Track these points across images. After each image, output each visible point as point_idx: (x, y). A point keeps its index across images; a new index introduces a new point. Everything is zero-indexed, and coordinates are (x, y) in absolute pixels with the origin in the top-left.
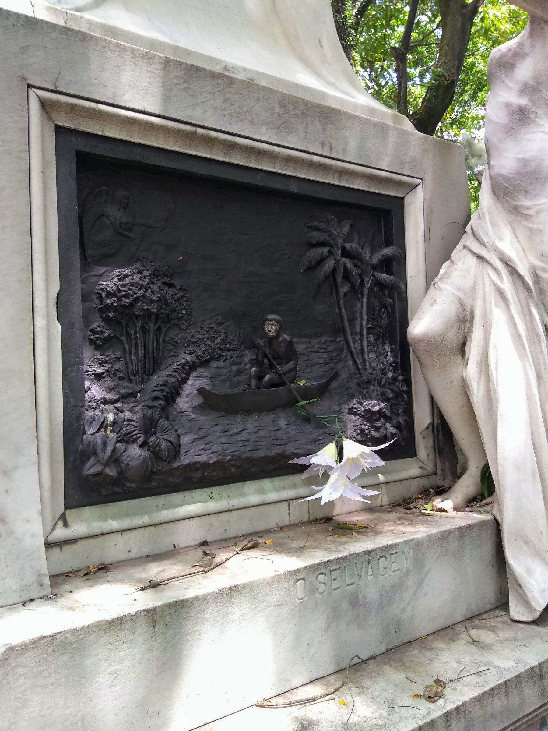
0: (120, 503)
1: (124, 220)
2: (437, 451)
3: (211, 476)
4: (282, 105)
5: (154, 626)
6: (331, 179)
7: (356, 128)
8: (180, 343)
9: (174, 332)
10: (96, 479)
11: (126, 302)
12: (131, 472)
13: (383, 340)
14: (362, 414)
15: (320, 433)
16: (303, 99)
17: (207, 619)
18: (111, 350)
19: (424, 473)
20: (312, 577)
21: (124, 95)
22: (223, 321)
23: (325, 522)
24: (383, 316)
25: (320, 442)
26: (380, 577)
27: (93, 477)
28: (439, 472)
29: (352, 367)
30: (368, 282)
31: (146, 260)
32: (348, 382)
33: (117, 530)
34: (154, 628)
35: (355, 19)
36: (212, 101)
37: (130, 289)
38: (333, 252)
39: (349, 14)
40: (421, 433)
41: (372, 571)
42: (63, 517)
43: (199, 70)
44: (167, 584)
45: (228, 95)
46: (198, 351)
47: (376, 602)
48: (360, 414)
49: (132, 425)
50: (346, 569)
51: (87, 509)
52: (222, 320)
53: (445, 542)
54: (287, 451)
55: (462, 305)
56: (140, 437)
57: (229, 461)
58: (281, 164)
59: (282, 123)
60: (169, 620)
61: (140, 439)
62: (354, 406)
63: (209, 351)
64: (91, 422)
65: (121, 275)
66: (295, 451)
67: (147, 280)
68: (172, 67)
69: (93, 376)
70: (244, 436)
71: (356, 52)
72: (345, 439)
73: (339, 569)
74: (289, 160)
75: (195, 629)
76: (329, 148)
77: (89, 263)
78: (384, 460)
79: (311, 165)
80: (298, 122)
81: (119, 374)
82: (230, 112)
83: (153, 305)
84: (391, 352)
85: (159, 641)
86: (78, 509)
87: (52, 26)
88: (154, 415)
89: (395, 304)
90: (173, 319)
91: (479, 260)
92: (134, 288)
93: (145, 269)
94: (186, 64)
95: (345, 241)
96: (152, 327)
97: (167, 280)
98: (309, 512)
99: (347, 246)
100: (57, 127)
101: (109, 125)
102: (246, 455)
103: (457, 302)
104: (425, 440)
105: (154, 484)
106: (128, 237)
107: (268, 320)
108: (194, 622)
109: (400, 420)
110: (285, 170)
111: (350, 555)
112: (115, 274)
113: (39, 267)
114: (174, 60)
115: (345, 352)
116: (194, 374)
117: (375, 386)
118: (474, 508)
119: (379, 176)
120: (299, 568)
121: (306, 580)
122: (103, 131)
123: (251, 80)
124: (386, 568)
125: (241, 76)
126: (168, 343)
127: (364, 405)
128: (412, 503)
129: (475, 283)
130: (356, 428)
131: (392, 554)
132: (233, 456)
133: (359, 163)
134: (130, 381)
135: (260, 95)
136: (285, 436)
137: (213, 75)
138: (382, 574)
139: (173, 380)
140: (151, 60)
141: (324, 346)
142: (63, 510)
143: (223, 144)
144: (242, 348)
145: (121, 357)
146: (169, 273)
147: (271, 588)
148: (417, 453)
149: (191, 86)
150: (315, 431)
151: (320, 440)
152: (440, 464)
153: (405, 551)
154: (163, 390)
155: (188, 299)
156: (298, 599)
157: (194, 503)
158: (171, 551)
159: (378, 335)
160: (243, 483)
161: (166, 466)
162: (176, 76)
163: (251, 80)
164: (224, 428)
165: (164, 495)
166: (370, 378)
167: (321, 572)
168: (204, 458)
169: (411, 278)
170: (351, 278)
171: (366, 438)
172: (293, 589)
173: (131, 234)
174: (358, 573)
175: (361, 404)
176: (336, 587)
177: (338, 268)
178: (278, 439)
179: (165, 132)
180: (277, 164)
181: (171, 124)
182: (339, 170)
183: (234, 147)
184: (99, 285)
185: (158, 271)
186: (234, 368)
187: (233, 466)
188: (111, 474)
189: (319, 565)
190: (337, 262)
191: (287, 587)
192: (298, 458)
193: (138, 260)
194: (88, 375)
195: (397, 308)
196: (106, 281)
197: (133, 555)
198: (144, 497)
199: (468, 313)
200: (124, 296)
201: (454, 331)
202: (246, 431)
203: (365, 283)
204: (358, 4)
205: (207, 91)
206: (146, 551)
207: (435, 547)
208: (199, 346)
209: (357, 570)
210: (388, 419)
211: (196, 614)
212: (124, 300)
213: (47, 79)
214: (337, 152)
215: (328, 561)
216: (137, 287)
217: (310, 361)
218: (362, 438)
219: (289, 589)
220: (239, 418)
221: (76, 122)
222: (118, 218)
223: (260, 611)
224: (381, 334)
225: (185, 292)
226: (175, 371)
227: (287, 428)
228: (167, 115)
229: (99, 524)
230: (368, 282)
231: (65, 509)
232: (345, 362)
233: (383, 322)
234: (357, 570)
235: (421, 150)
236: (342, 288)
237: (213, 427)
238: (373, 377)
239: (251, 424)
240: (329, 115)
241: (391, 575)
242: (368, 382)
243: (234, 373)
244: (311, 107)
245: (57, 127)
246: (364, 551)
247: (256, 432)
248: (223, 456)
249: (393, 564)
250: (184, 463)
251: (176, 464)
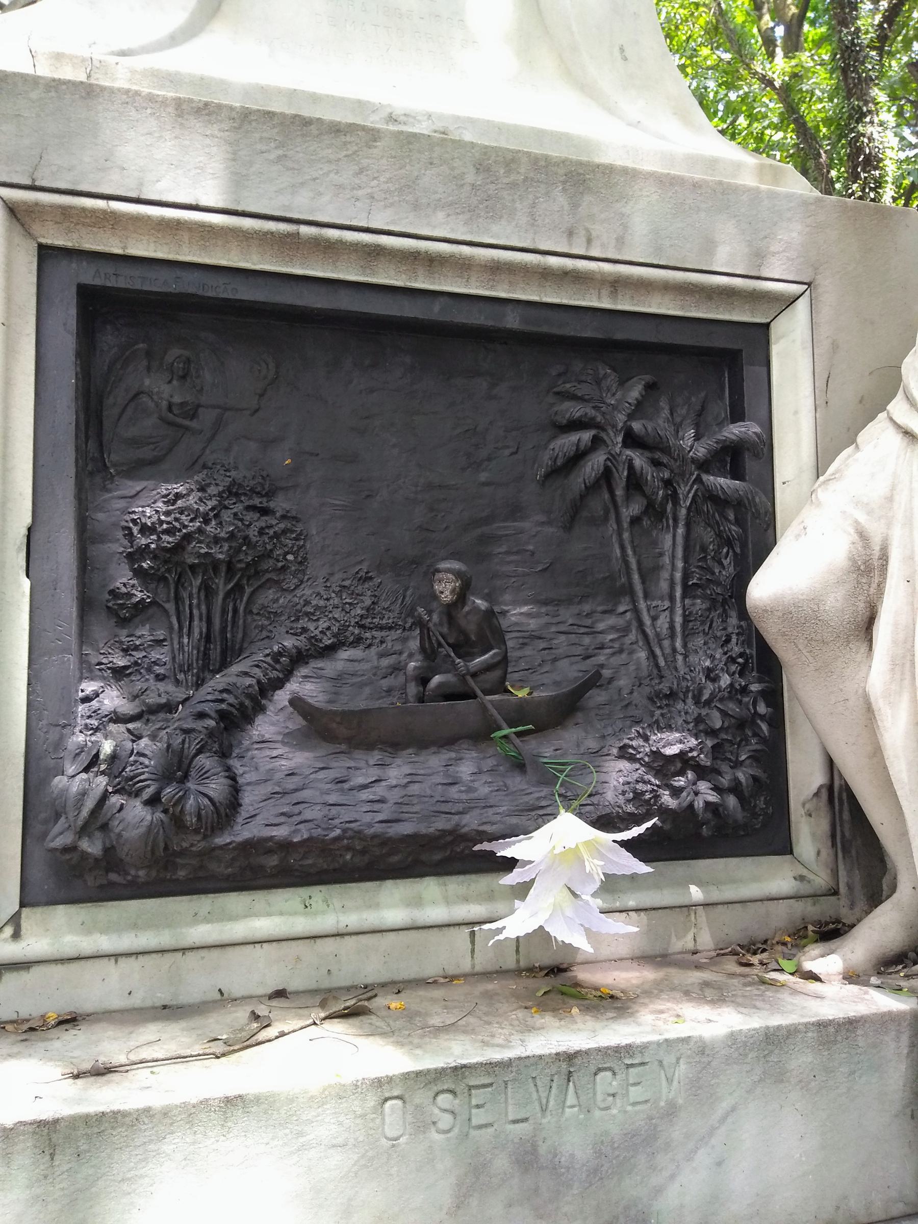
0: (124, 903)
1: (177, 399)
2: (839, 845)
3: (301, 866)
4: (481, 167)
5: (52, 1156)
6: (595, 298)
7: (648, 196)
8: (282, 614)
9: (271, 594)
10: (67, 857)
11: (168, 543)
12: (126, 849)
13: (725, 611)
14: (647, 759)
15: (542, 794)
16: (528, 154)
17: (168, 1155)
18: (148, 626)
19: (805, 889)
20: (421, 1097)
21: (158, 181)
22: (370, 574)
23: (547, 975)
24: (726, 562)
25: (541, 812)
26: (597, 1113)
27: (61, 853)
28: (843, 889)
29: (644, 663)
30: (686, 492)
31: (218, 467)
32: (631, 693)
33: (109, 953)
34: (52, 1159)
35: (876, 30)
36: (332, 175)
37: (176, 520)
38: (605, 438)
39: (864, 25)
40: (804, 805)
41: (578, 1098)
42: (15, 920)
43: (306, 122)
44: (127, 1071)
45: (365, 162)
46: (312, 629)
47: (584, 1165)
48: (642, 759)
49: (141, 764)
50: (510, 1086)
51: (61, 909)
52: (367, 573)
53: (776, 1051)
54: (464, 826)
55: (863, 536)
56: (148, 786)
57: (337, 839)
58: (482, 279)
59: (481, 202)
60: (85, 1147)
61: (147, 790)
62: (631, 743)
63: (335, 629)
64: (78, 755)
65: (168, 495)
66: (481, 828)
67: (210, 504)
68: (254, 124)
69: (109, 671)
70: (379, 791)
71: (880, 89)
72: (562, 811)
73: (491, 1085)
74: (495, 269)
75: (142, 1171)
76: (584, 239)
77: (113, 476)
78: (645, 860)
79: (546, 275)
80: (516, 197)
81: (159, 670)
82: (369, 191)
83: (221, 547)
84: (738, 634)
85: (61, 1186)
86: (45, 908)
87: (32, 81)
88: (186, 745)
89: (746, 537)
90: (267, 571)
91: (906, 440)
92: (183, 517)
93: (213, 482)
94: (283, 115)
95: (631, 417)
96: (221, 586)
97: (256, 501)
98: (517, 951)
99: (636, 426)
100: (42, 248)
101: (135, 235)
102: (372, 831)
103: (852, 531)
104: (812, 819)
105: (181, 874)
106: (187, 428)
107: (438, 571)
108: (139, 1157)
109: (741, 776)
110: (492, 288)
111: (520, 1058)
112: (159, 493)
114: (259, 110)
115: (633, 636)
116: (304, 671)
117: (685, 704)
118: (892, 980)
119: (702, 284)
120: (391, 1074)
121: (408, 1100)
122: (124, 248)
123: (444, 133)
124: (614, 1095)
125: (422, 128)
126: (258, 614)
127: (651, 742)
128: (762, 952)
129: (893, 488)
130: (626, 788)
131: (632, 1065)
132: (345, 831)
133: (655, 262)
134: (177, 682)
135: (435, 155)
136: (464, 796)
137: (336, 129)
138: (602, 1105)
139: (248, 681)
140: (214, 116)
141: (588, 622)
142: (17, 908)
143: (356, 251)
144: (407, 626)
145: (164, 640)
146: (264, 489)
147: (320, 1110)
148: (794, 846)
149: (290, 153)
150: (533, 789)
151: (542, 807)
152: (845, 873)
153: (665, 1063)
154: (222, 701)
155: (300, 534)
156: (386, 1138)
157: (269, 914)
158: (215, 1002)
159: (714, 601)
160: (378, 883)
161: (199, 841)
162: (261, 138)
163: (444, 133)
164: (339, 776)
165: (212, 895)
166: (675, 686)
167: (445, 1087)
168: (281, 832)
169: (784, 483)
170: (644, 488)
171: (647, 810)
172: (374, 1116)
173: (194, 424)
174: (540, 1099)
175: (646, 739)
176: (482, 1121)
177: (614, 470)
178: (447, 802)
179: (239, 239)
180: (473, 279)
181: (272, 226)
182: (609, 279)
183: (378, 254)
184: (130, 513)
185: (240, 486)
186: (386, 662)
187: (348, 848)
188: (90, 850)
189: (440, 1073)
190: (612, 458)
191: (359, 1111)
192: (490, 841)
193: (205, 467)
194: (100, 670)
195: (750, 546)
196: (143, 507)
197: (137, 1001)
198: (173, 896)
199: (876, 553)
200: (166, 532)
201: (844, 592)
202: (384, 784)
203: (681, 496)
204: (884, 5)
205: (323, 158)
206: (163, 996)
207: (748, 1060)
208: (318, 620)
209: (537, 1091)
210: (702, 773)
211: (145, 1143)
212: (165, 537)
213: (18, 169)
214: (603, 246)
215: (464, 1066)
216: (189, 515)
217: (553, 651)
218: (637, 808)
219: (363, 1116)
220: (376, 756)
221: (75, 236)
222: (165, 395)
223: (292, 1153)
224: (720, 598)
225: (294, 523)
226: (257, 666)
227: (473, 781)
228: (240, 208)
229: (75, 938)
230: (686, 492)
231: (22, 905)
232: (631, 653)
233: (724, 573)
234: (537, 1091)
235: (808, 226)
236: (627, 507)
237: (316, 772)
238: (684, 684)
239: (396, 773)
240: (588, 176)
241: (626, 1112)
242: (672, 695)
243: (384, 671)
244: (547, 167)
245: (42, 248)
246: (557, 1054)
247: (405, 786)
248: (324, 829)
249: (632, 1089)
250: (239, 839)
251: (220, 841)
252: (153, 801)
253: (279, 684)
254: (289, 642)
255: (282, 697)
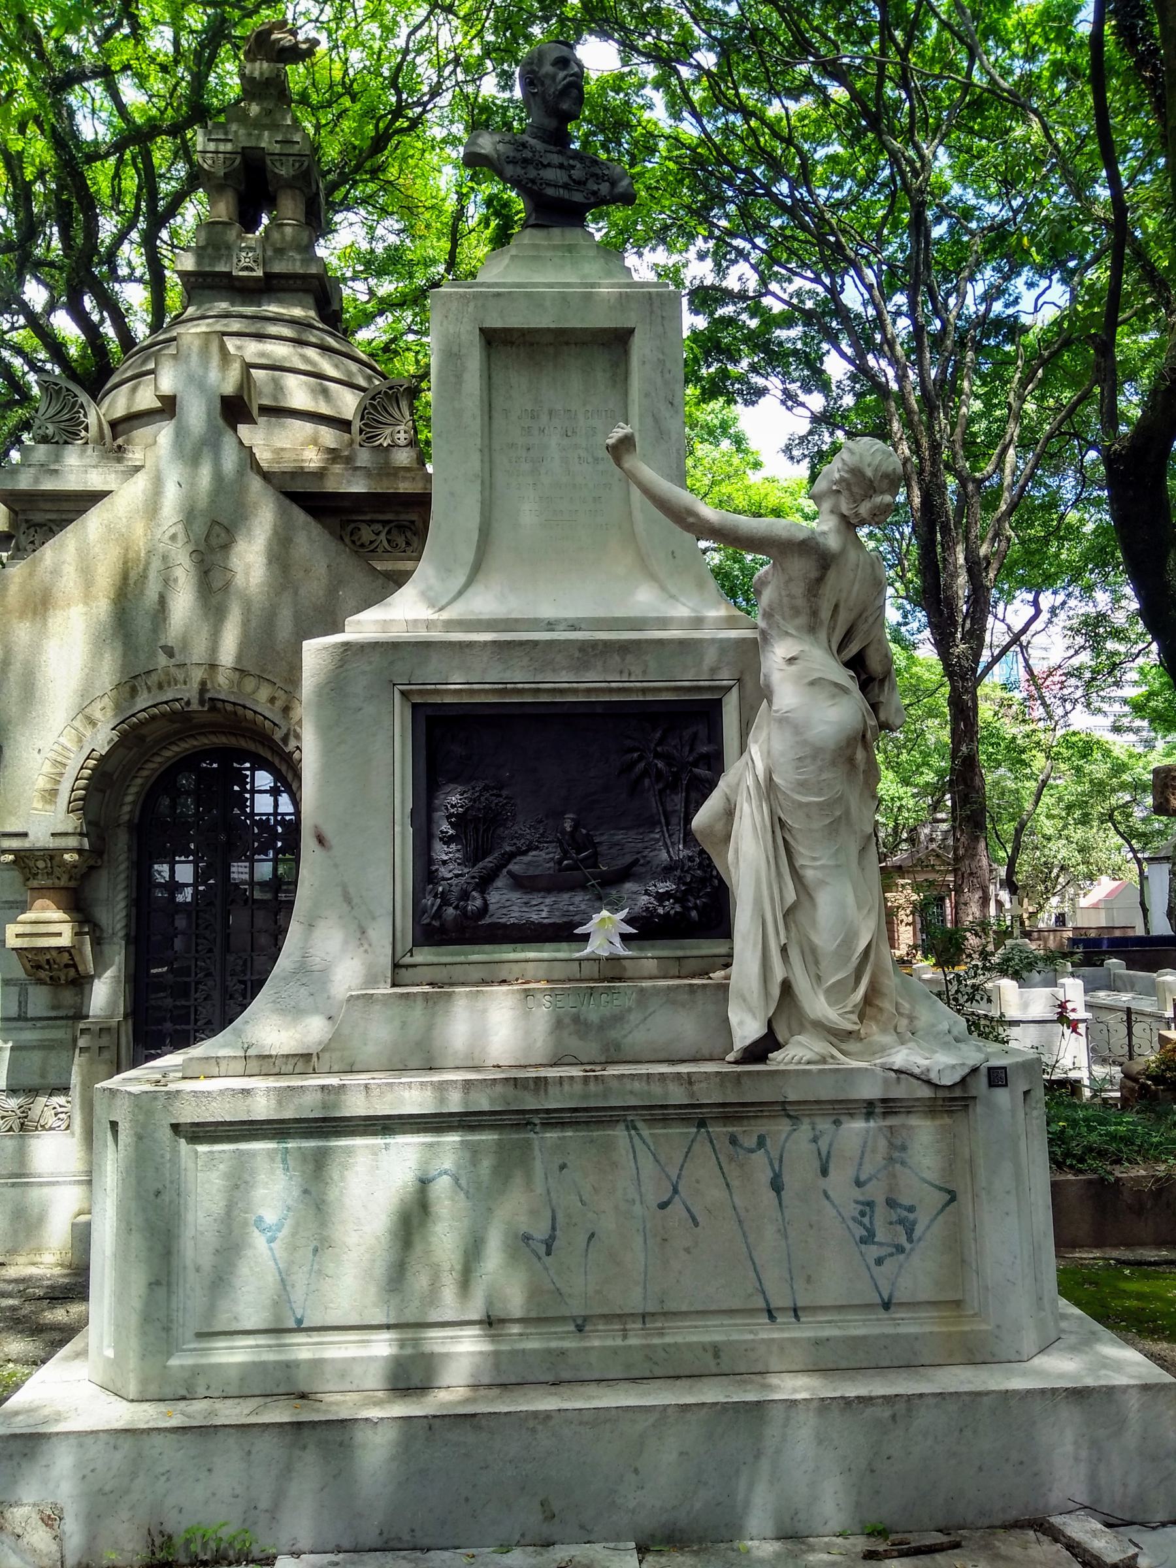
42: (411, 951)
55: (728, 800)
79: (611, 691)
95: (657, 745)
113: (398, 795)
252: (456, 908)
253: (505, 866)
254: (508, 849)
255: (505, 871)
